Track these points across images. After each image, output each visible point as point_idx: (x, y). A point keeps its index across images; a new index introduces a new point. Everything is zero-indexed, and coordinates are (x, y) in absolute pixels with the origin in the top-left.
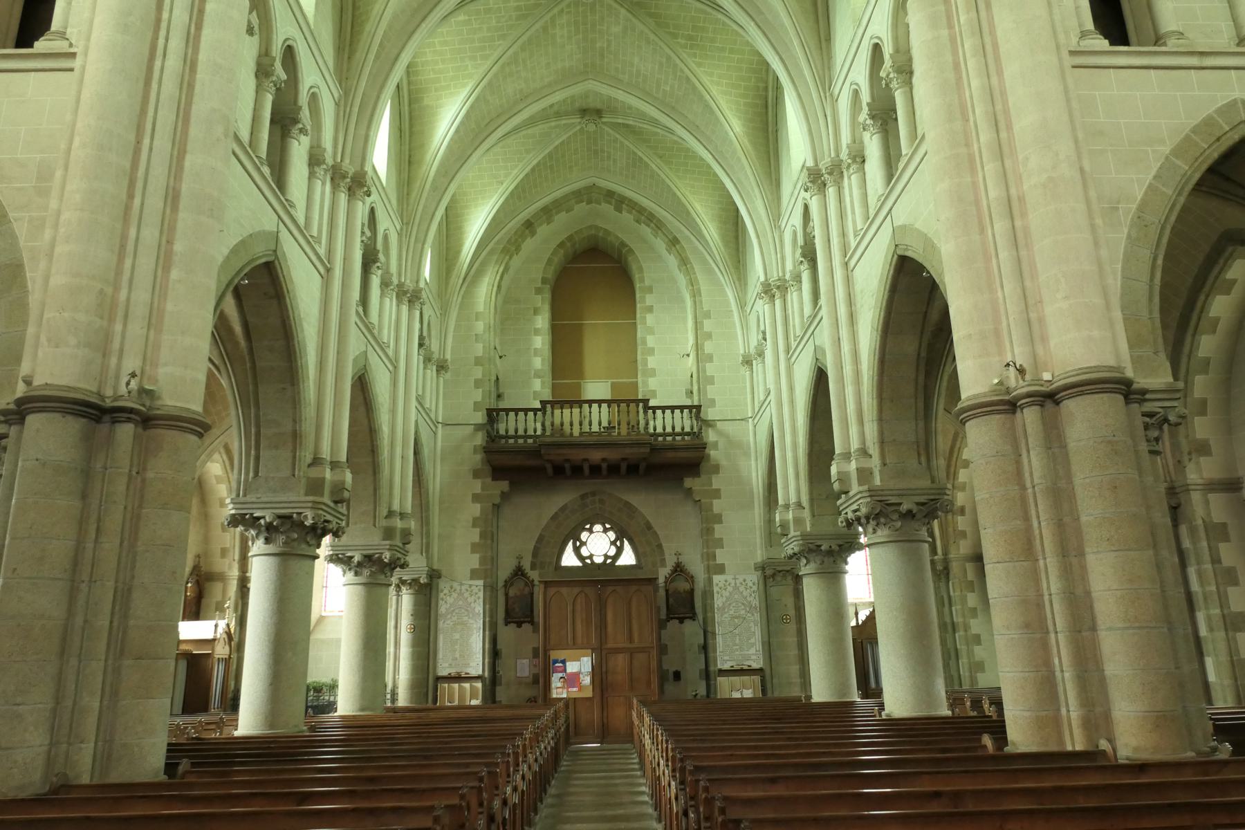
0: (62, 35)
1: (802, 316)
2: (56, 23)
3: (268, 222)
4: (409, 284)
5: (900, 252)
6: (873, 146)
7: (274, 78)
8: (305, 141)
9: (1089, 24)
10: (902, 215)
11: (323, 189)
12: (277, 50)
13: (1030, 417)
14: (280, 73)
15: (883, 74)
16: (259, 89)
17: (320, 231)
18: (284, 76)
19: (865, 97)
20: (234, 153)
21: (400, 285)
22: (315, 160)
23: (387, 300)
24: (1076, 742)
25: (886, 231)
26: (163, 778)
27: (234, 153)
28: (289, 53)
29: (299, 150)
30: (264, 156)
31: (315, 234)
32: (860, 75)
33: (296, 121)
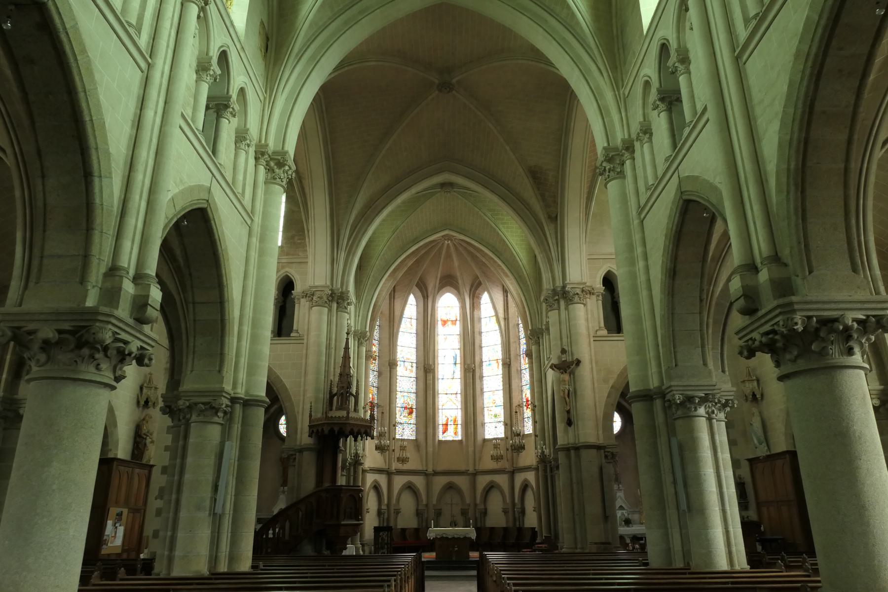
0: (297, 332)
1: (654, 167)
2: (295, 328)
3: (203, 177)
4: (272, 144)
5: (685, 197)
6: (660, 122)
7: (212, 72)
8: (235, 122)
9: (602, 324)
10: (686, 170)
11: (247, 159)
12: (214, 54)
13: (572, 452)
14: (215, 68)
15: (670, 63)
16: (199, 80)
17: (141, 18)
18: (219, 72)
19: (655, 84)
20: (180, 127)
21: (355, 332)
22: (241, 137)
23: (243, 155)
24: (679, 564)
25: (675, 180)
26: (251, 570)
27: (180, 127)
28: (223, 57)
29: (228, 127)
30: (201, 128)
31: (134, 21)
32: (650, 70)
33: (227, 106)
